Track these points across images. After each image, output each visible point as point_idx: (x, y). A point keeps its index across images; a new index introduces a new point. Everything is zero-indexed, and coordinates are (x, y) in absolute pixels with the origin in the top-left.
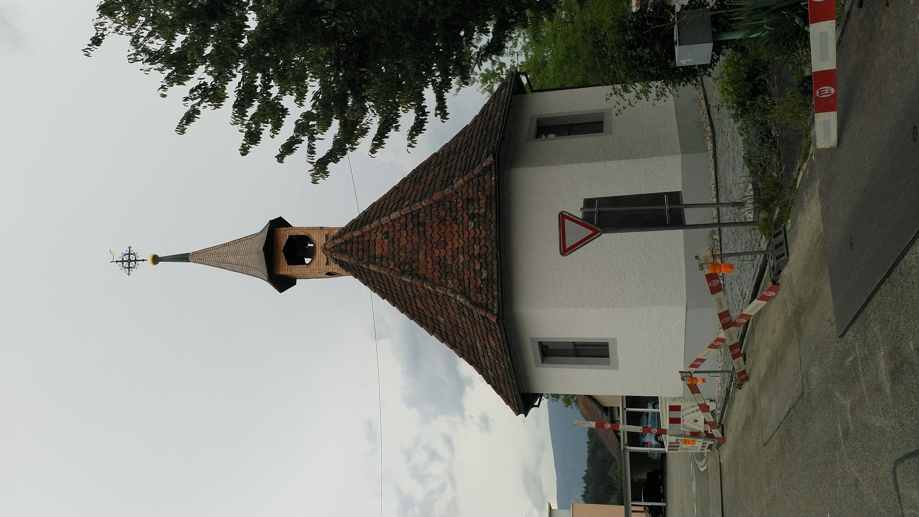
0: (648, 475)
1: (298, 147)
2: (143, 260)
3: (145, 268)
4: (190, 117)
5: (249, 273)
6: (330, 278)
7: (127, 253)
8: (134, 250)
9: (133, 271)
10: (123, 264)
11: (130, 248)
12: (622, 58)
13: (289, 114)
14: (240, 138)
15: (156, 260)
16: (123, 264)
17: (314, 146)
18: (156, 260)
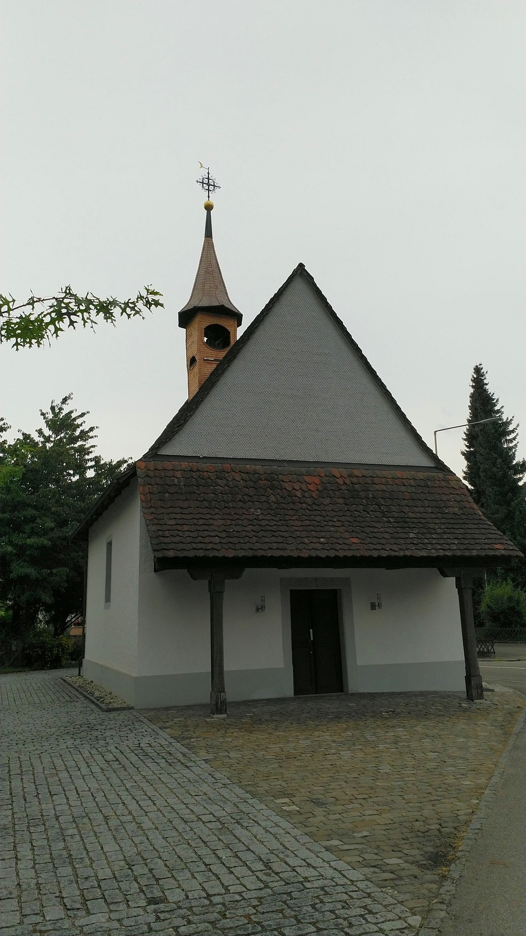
0: (205, 336)
1: (93, 446)
2: (209, 197)
3: (202, 197)
4: (65, 400)
5: (217, 270)
6: (183, 309)
7: (215, 184)
8: (217, 190)
9: (200, 186)
10: (206, 178)
11: (197, 181)
12: (330, 706)
13: (493, 394)
14: (43, 411)
15: (209, 208)
16: (206, 178)
17: (481, 366)
18: (209, 208)
